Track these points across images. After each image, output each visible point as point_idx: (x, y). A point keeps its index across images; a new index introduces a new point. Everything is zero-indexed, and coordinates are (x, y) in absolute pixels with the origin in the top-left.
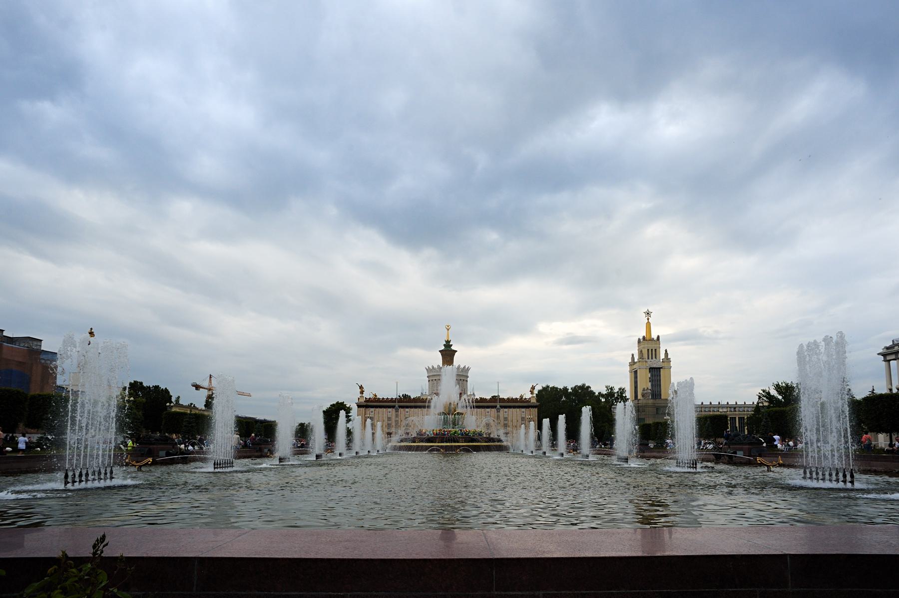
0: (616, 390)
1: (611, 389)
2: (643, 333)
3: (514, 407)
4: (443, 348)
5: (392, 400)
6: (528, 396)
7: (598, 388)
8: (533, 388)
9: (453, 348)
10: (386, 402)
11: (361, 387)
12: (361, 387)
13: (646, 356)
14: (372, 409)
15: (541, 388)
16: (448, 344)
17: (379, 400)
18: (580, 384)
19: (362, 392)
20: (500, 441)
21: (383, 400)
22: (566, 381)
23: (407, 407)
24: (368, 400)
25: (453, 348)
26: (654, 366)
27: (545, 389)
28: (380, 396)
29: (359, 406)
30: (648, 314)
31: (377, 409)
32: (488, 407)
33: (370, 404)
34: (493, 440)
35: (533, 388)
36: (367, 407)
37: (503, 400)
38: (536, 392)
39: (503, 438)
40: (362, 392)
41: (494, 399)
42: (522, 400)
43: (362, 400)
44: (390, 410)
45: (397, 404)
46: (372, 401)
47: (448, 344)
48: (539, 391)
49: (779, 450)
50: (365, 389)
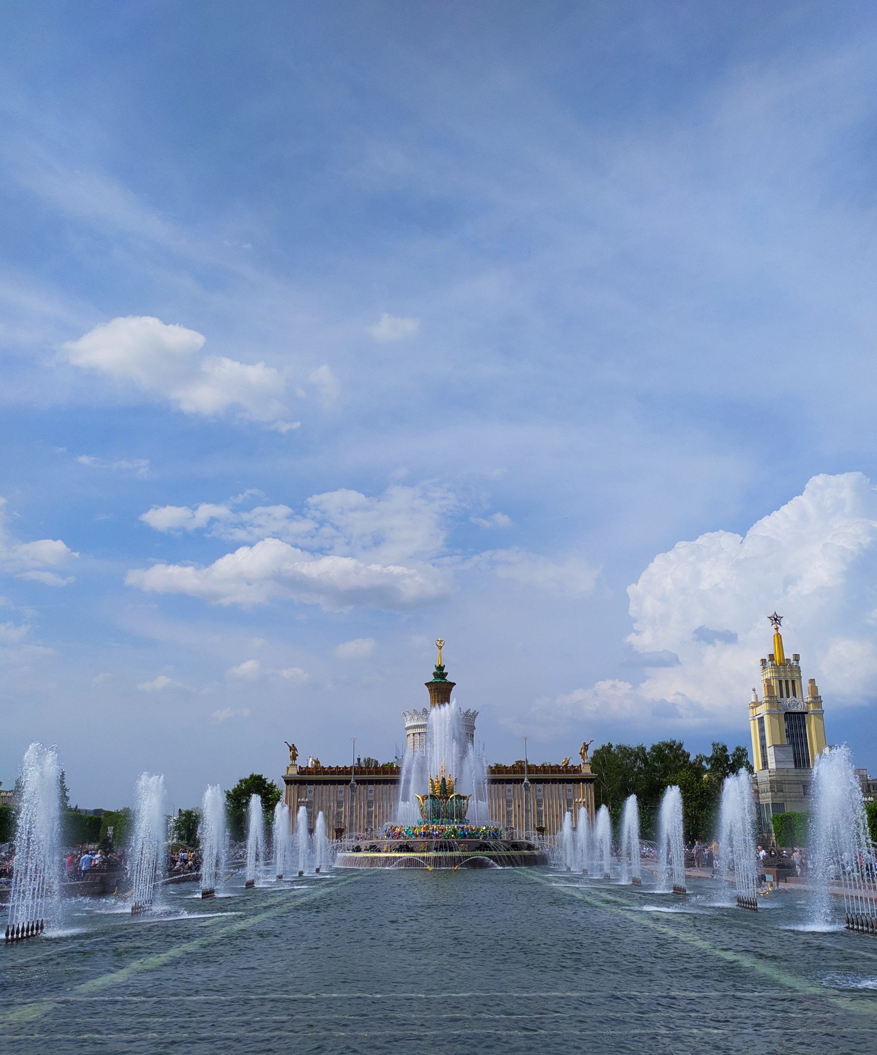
0: (730, 752)
1: (724, 749)
2: (767, 649)
3: (554, 781)
4: (431, 678)
5: (346, 771)
6: (576, 761)
7: (697, 750)
8: (586, 747)
9: (449, 678)
10: (333, 773)
11: (293, 748)
12: (293, 748)
13: (776, 692)
14: (311, 787)
15: (599, 747)
16: (440, 672)
17: (323, 771)
18: (667, 740)
19: (294, 757)
20: (530, 847)
21: (331, 771)
22: (646, 736)
23: (371, 782)
24: (303, 771)
25: (449, 678)
26: (795, 710)
27: (607, 749)
28: (325, 764)
29: (288, 782)
30: (754, 690)
31: (319, 787)
32: (509, 781)
33: (310, 779)
34: (516, 846)
35: (586, 747)
36: (302, 782)
37: (532, 769)
38: (590, 753)
39: (534, 840)
40: (294, 757)
41: (519, 767)
42: (567, 769)
43: (294, 771)
44: (341, 787)
45: (352, 778)
46: (310, 773)
47: (440, 672)
48: (596, 752)
49: (266, 894)
50: (299, 752)
